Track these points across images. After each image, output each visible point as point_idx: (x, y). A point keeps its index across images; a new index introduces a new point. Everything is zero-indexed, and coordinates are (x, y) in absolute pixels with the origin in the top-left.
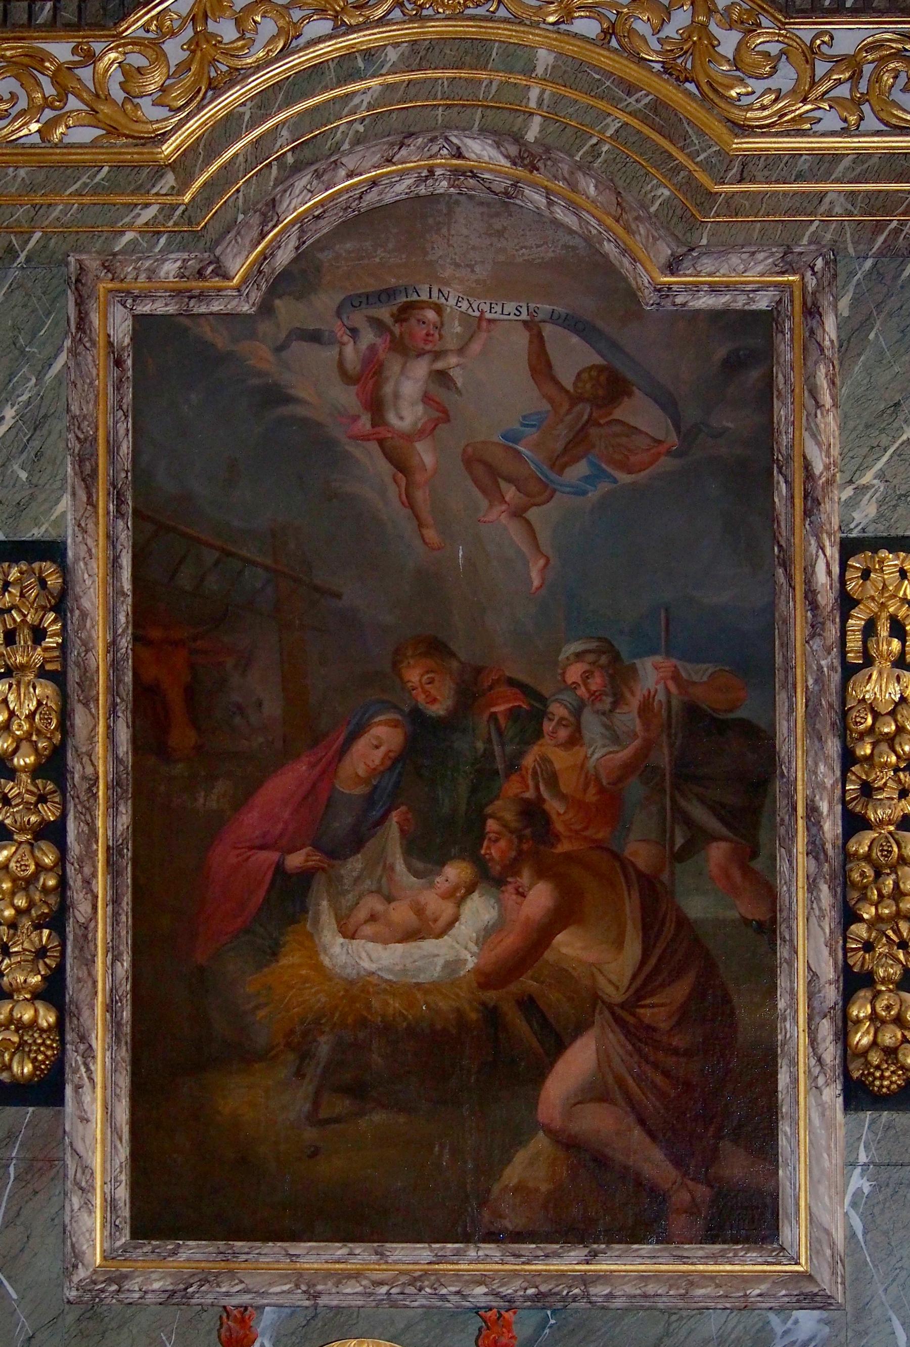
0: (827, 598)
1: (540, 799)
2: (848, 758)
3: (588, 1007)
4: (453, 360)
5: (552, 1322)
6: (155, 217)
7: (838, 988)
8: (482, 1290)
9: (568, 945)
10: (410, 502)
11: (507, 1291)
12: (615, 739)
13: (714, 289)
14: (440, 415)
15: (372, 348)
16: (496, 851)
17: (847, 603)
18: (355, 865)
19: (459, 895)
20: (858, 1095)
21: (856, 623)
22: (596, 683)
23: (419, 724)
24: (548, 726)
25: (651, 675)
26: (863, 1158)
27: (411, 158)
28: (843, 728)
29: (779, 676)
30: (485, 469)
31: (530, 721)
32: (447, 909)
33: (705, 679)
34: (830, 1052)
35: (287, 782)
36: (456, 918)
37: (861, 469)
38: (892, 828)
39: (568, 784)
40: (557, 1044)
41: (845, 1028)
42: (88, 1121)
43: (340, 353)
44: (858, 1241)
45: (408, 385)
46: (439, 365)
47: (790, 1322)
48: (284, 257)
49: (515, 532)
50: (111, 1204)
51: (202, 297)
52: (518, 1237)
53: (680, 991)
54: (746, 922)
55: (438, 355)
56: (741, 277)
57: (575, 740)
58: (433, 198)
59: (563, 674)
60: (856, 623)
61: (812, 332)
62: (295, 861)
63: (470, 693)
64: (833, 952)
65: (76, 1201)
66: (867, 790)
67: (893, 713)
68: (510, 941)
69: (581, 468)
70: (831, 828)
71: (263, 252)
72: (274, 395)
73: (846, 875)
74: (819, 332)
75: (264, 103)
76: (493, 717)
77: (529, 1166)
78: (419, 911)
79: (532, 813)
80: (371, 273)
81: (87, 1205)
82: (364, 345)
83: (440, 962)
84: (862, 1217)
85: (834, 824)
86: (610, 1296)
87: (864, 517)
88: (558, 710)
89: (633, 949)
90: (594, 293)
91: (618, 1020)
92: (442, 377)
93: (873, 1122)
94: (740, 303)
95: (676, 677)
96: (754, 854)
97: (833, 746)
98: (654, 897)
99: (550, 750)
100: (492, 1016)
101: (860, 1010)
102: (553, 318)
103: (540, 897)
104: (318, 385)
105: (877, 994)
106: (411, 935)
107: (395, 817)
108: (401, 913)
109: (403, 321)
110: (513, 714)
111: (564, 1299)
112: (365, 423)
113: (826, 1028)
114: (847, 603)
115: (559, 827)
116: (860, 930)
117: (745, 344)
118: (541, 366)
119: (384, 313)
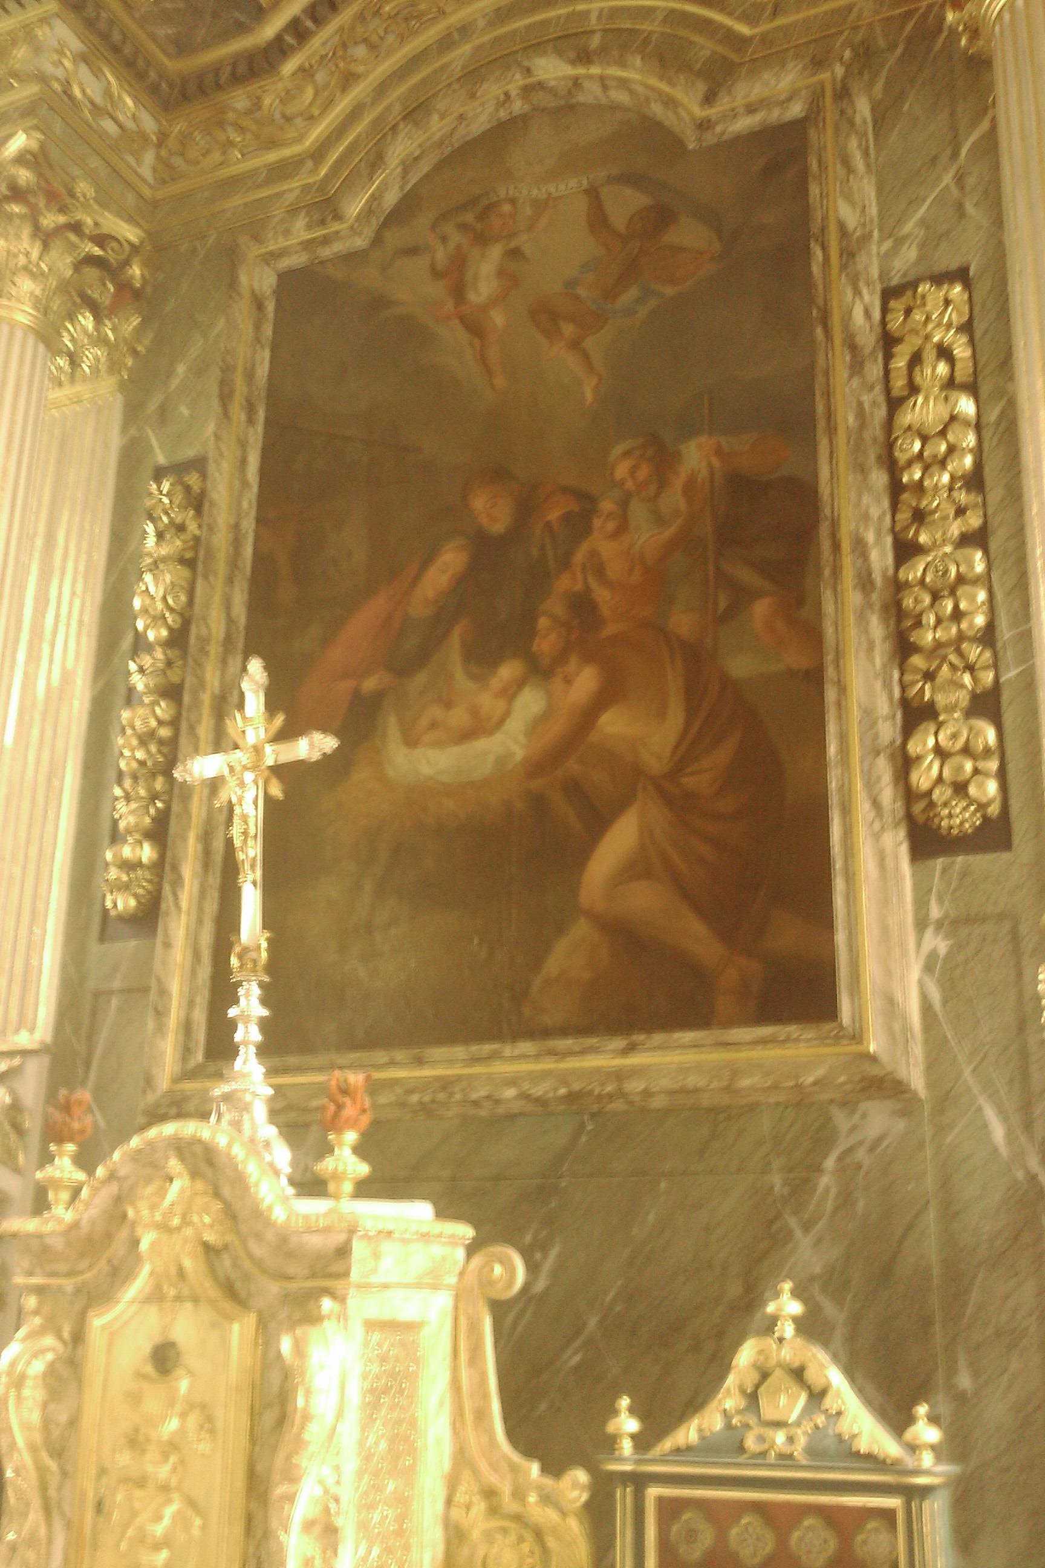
0: (868, 339)
1: (588, 590)
2: (896, 489)
3: (630, 780)
4: (524, 237)
5: (590, 1127)
6: (298, 197)
7: (894, 725)
8: (510, 1093)
9: (614, 724)
10: (483, 360)
11: (538, 1091)
12: (660, 520)
13: (751, 109)
14: (509, 279)
15: (459, 247)
16: (546, 644)
17: (889, 342)
18: (421, 678)
19: (510, 693)
20: (926, 840)
21: (900, 363)
22: (643, 473)
24: (597, 523)
25: (696, 457)
26: (935, 912)
27: (492, 90)
28: (893, 468)
29: (821, 424)
30: (546, 316)
31: (580, 523)
32: (501, 705)
34: (888, 794)
35: (364, 620)
36: (507, 713)
37: (900, 221)
38: (948, 549)
39: (615, 570)
40: (598, 822)
41: (905, 764)
43: (433, 258)
44: (936, 1015)
46: (513, 244)
47: (857, 1116)
48: (391, 198)
49: (572, 362)
50: (187, 1028)
51: (326, 240)
52: (563, 1032)
53: (723, 755)
54: (792, 673)
55: (512, 235)
56: (776, 92)
57: (623, 528)
58: (513, 120)
59: (612, 474)
60: (900, 363)
61: (842, 112)
62: (370, 684)
63: (526, 508)
64: (887, 685)
65: (150, 1025)
66: (920, 516)
67: (943, 433)
68: (557, 728)
69: (632, 293)
70: (881, 558)
71: (373, 195)
72: (380, 302)
73: (898, 604)
74: (849, 111)
75: (381, 89)
76: (548, 525)
77: (572, 953)
78: (475, 712)
79: (583, 607)
81: (160, 1029)
82: (452, 246)
83: (491, 759)
84: (940, 982)
85: (883, 555)
86: (647, 1093)
88: (607, 505)
89: (676, 718)
90: (644, 145)
91: (659, 789)
92: (515, 254)
93: (944, 870)
94: (775, 116)
95: (719, 452)
96: (800, 602)
97: (879, 478)
98: (696, 659)
99: (601, 543)
100: (539, 804)
101: (924, 742)
102: (610, 180)
103: (585, 681)
104: (414, 287)
105: (940, 725)
106: (467, 735)
107: (457, 632)
108: (459, 717)
110: (567, 518)
111: (599, 1097)
112: (450, 306)
113: (884, 769)
114: (889, 342)
115: (605, 611)
116: (917, 661)
117: (782, 157)
118: (598, 220)
119: (469, 218)
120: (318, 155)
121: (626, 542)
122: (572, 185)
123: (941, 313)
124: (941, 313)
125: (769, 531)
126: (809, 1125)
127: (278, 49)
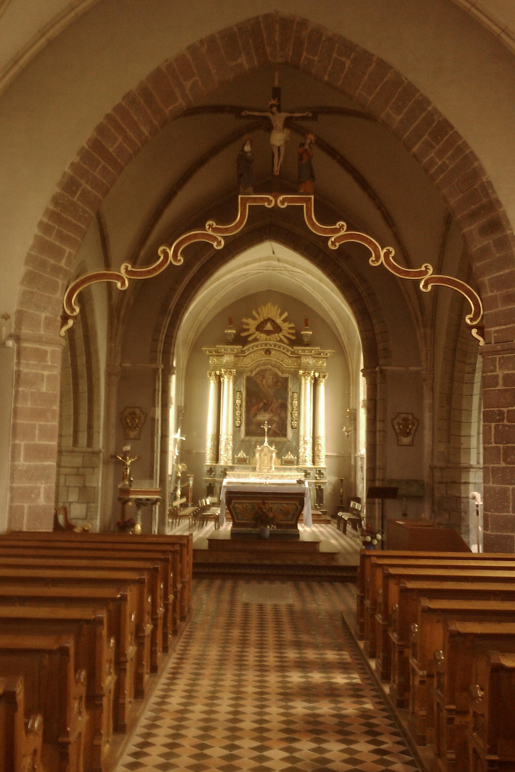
20: (292, 428)
23: (265, 404)
30: (269, 387)
33: (233, 501)
35: (255, 407)
42: (211, 468)
45: (264, 381)
56: (285, 375)
63: (268, 401)
72: (255, 381)
80: (262, 373)
87: (293, 391)
90: (276, 375)
104: (258, 381)
109: (263, 377)
117: (286, 379)
118: (273, 380)
120: (250, 367)
121: (275, 405)
122: (271, 377)
123: (296, 395)
124: (296, 395)
125: (284, 406)
126: (285, 443)
127: (245, 356)
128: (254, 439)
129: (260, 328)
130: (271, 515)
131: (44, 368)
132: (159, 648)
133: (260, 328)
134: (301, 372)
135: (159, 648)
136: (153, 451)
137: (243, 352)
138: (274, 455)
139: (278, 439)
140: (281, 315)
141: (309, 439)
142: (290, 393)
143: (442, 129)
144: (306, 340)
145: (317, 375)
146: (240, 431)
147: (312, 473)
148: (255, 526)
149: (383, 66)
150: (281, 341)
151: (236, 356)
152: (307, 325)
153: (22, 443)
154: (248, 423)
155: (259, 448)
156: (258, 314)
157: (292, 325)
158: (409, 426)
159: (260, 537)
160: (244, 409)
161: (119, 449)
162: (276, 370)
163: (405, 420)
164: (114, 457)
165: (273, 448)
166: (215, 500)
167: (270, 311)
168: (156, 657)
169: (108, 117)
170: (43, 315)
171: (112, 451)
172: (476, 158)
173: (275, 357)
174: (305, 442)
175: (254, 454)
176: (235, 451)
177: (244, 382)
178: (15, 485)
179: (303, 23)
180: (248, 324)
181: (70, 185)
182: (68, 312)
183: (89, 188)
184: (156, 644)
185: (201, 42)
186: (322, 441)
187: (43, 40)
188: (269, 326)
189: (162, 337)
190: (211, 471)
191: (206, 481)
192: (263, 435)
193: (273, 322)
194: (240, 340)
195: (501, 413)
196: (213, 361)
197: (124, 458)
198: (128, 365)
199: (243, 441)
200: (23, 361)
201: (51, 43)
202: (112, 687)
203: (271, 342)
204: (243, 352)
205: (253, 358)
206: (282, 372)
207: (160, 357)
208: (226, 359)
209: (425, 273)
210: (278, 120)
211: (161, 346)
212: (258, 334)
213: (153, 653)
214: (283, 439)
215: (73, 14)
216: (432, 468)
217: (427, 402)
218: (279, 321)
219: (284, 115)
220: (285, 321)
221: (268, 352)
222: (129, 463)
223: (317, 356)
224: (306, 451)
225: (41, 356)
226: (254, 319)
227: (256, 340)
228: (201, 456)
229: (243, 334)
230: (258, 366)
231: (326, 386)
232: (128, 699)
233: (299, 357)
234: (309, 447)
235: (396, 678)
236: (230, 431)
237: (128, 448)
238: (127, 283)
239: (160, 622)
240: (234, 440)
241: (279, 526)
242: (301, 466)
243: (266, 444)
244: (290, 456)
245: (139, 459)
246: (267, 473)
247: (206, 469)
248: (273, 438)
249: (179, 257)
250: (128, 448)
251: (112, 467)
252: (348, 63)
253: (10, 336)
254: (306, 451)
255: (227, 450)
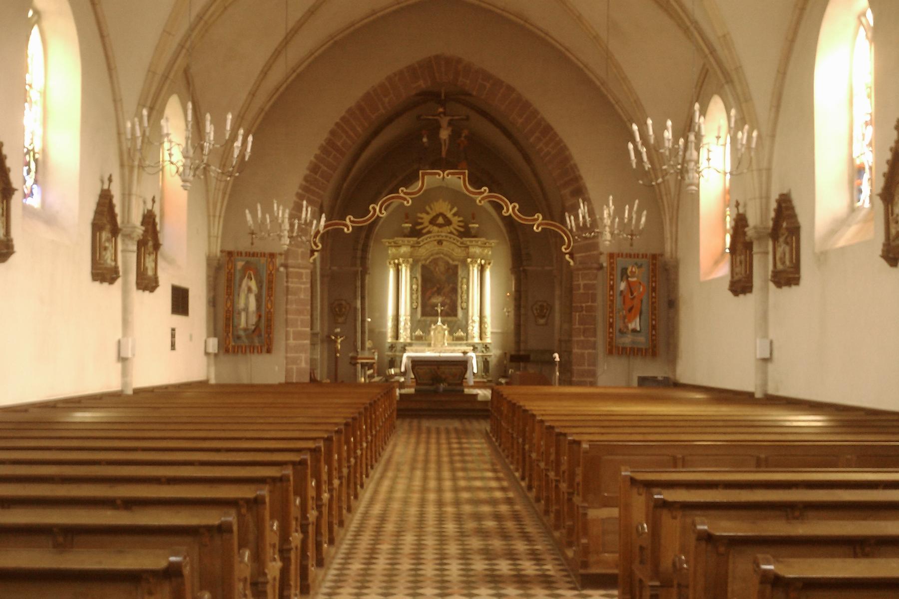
56: (456, 263)
80: (435, 262)
90: (447, 263)
104: (432, 268)
109: (437, 264)
121: (447, 289)
123: (465, 280)
124: (465, 280)
125: (454, 290)
126: (456, 322)
128: (429, 319)
129: (433, 222)
130: (443, 376)
131: (301, 283)
132: (325, 538)
133: (433, 222)
134: (469, 260)
135: (325, 538)
136: (356, 332)
137: (418, 243)
138: (446, 332)
139: (449, 319)
140: (451, 210)
141: (477, 318)
142: (460, 279)
143: (547, 130)
144: (473, 232)
145: (483, 262)
146: (416, 312)
147: (479, 347)
148: (432, 385)
149: (510, 89)
150: (451, 233)
151: (412, 246)
152: (474, 218)
153: (291, 330)
154: (424, 306)
155: (433, 327)
156: (431, 209)
157: (461, 219)
158: (545, 311)
159: (436, 392)
160: (420, 293)
161: (331, 332)
162: (447, 258)
163: (542, 306)
164: (329, 337)
165: (445, 327)
166: (397, 370)
167: (442, 207)
168: (321, 549)
169: (337, 124)
170: (300, 250)
171: (326, 334)
172: (568, 149)
173: (446, 247)
174: (473, 321)
175: (429, 332)
176: (413, 330)
177: (419, 270)
178: (289, 355)
179: (459, 61)
180: (422, 218)
181: (314, 169)
182: (314, 248)
183: (325, 168)
184: (321, 534)
185: (395, 74)
186: (488, 320)
187: (294, 75)
188: (441, 220)
189: (360, 247)
190: (392, 347)
191: (388, 356)
192: (436, 315)
193: (445, 217)
194: (416, 233)
195: (582, 307)
196: (392, 251)
197: (336, 337)
198: (335, 268)
199: (419, 321)
200: (290, 280)
201: (299, 76)
202: (277, 574)
203: (443, 234)
204: (418, 243)
205: (427, 248)
206: (453, 260)
207: (359, 262)
208: (404, 250)
209: (537, 219)
210: (444, 121)
211: (359, 253)
212: (431, 228)
213: (318, 546)
214: (453, 319)
215: (313, 57)
216: (560, 341)
217: (557, 292)
218: (449, 215)
219: (448, 118)
220: (454, 215)
221: (440, 242)
222: (339, 341)
223: (483, 246)
224: (474, 329)
225: (300, 276)
226: (428, 213)
227: (429, 232)
228: (383, 335)
229: (419, 227)
230: (432, 255)
231: (491, 272)
232: (293, 591)
233: (467, 247)
234: (477, 325)
235: (527, 479)
236: (408, 313)
237: (338, 330)
238: (351, 229)
239: (325, 510)
240: (411, 320)
241: (449, 384)
242: (470, 341)
243: (439, 323)
244: (461, 333)
245: (346, 338)
246: (440, 347)
247: (388, 345)
248: (445, 318)
249: (383, 211)
250: (338, 330)
251: (326, 345)
252: (488, 85)
253: (282, 265)
254: (474, 329)
255: (405, 329)
